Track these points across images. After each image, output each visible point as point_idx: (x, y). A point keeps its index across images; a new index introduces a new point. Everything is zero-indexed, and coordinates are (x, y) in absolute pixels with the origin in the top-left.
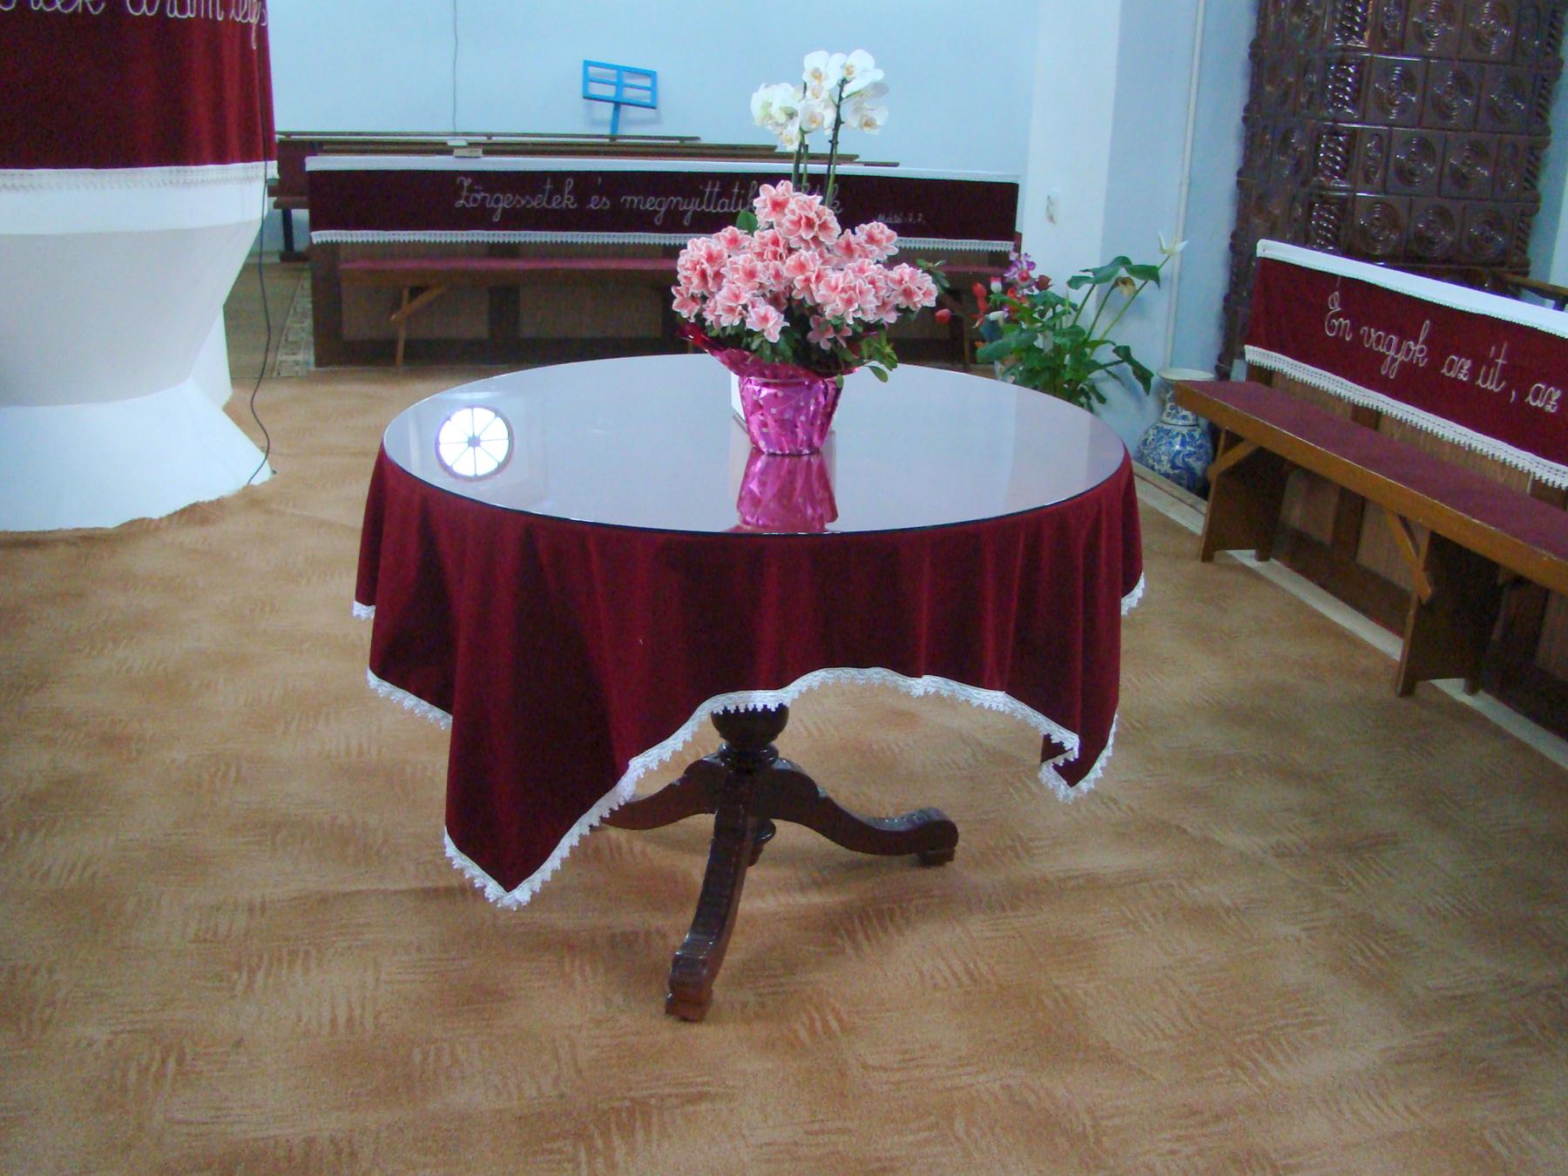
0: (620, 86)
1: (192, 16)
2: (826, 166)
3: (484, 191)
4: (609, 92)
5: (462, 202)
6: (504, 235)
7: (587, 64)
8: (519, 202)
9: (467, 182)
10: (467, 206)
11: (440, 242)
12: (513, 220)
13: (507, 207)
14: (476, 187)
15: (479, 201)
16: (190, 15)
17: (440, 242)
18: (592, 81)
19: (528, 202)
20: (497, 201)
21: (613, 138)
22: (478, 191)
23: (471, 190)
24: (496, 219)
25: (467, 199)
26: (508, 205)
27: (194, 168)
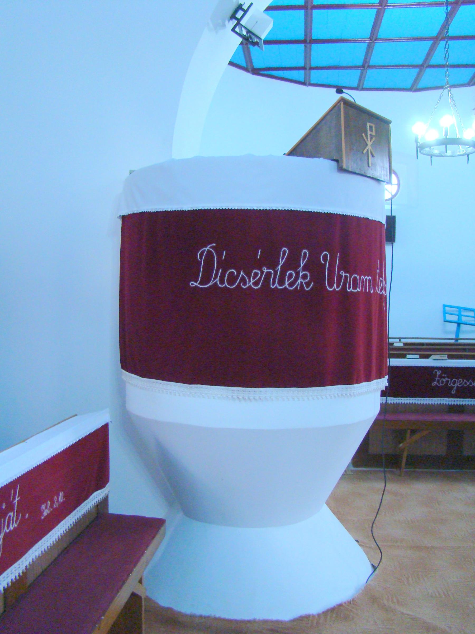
0: (459, 316)
1: (359, 290)
2: (461, 336)
3: (448, 377)
4: (455, 318)
5: (435, 383)
6: (452, 400)
7: (445, 306)
8: (466, 383)
9: (439, 373)
10: (438, 385)
11: (423, 404)
12: (462, 393)
13: (459, 385)
14: (443, 375)
15: (445, 382)
16: (358, 290)
17: (423, 404)
18: (447, 314)
19: (471, 384)
20: (454, 383)
21: (457, 340)
22: (444, 378)
23: (441, 377)
24: (453, 392)
25: (438, 381)
26: (459, 385)
27: (355, 385)
